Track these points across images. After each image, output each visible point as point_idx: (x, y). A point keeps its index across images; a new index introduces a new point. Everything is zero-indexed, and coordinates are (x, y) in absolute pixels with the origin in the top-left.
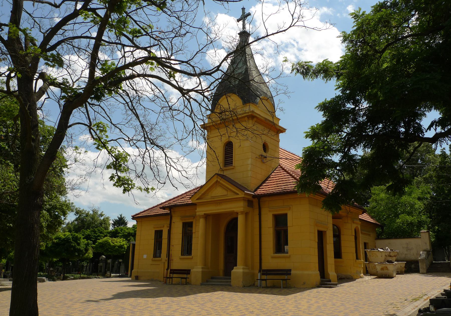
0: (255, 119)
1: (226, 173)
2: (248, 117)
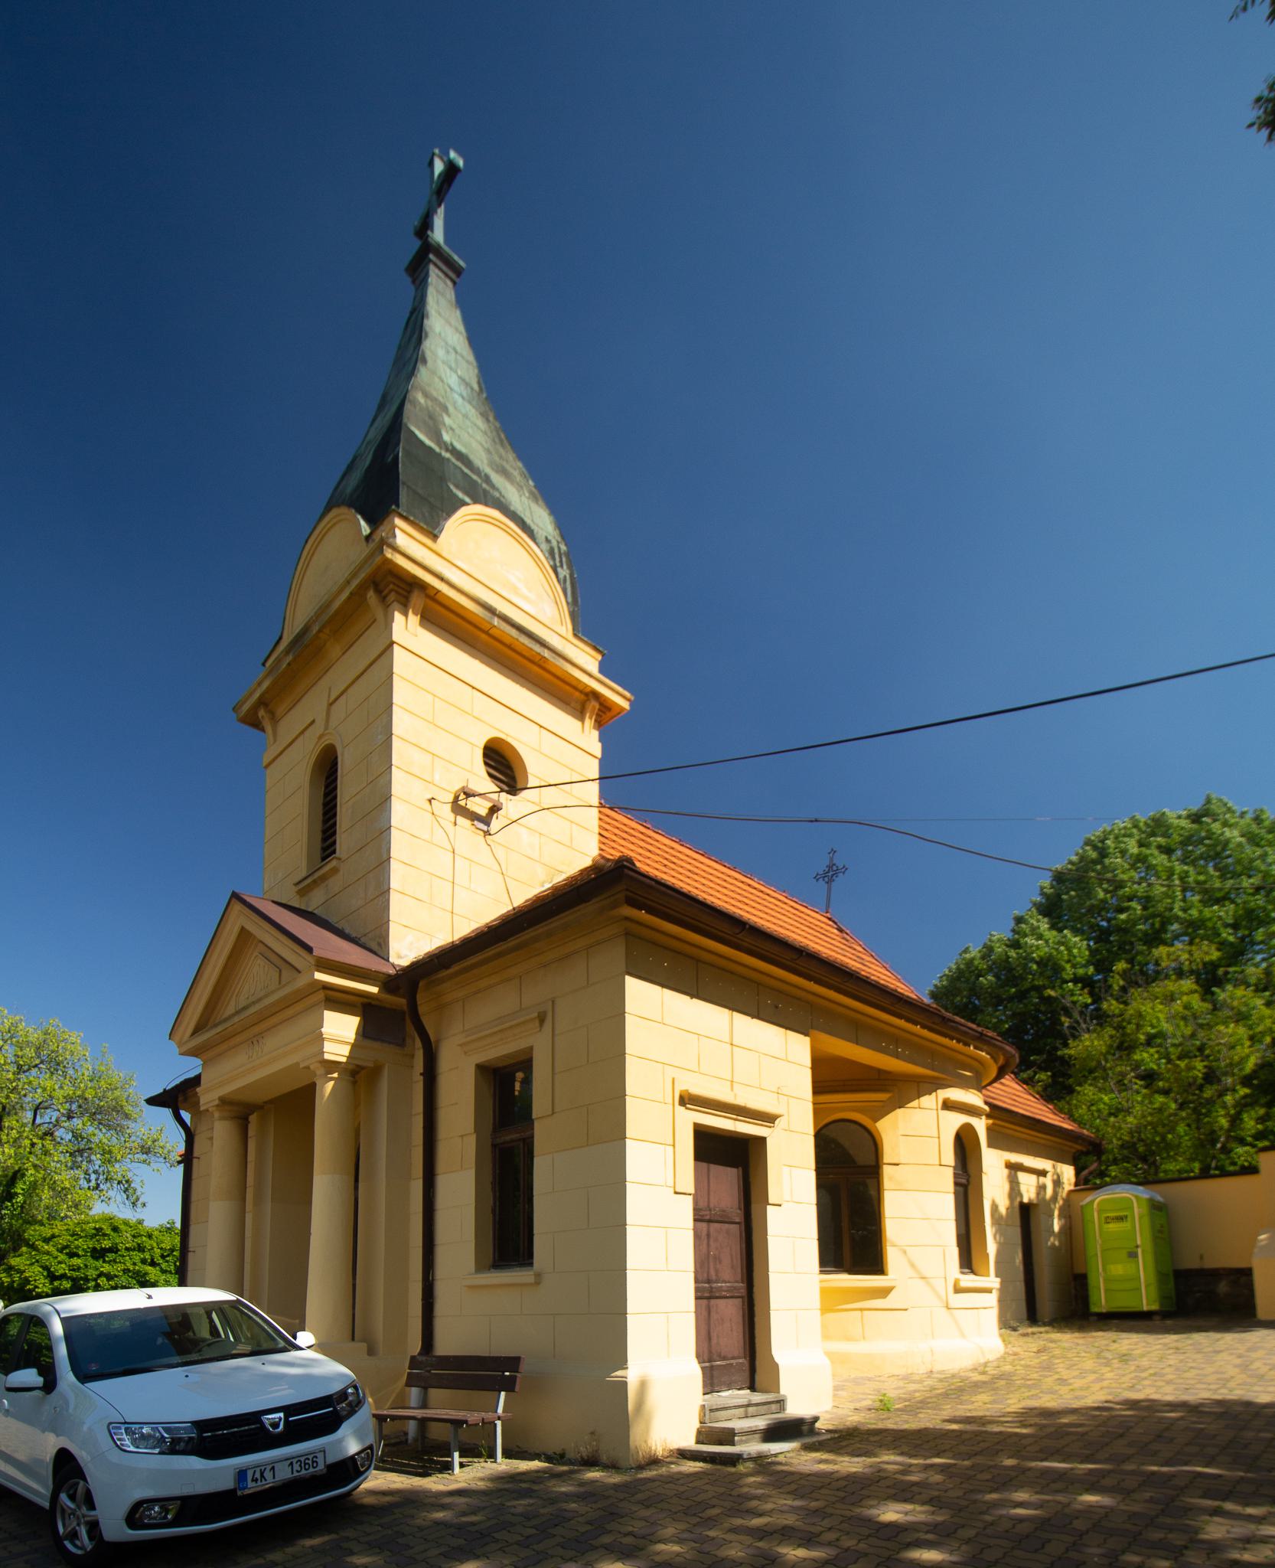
0: (417, 599)
1: (315, 902)
2: (378, 591)
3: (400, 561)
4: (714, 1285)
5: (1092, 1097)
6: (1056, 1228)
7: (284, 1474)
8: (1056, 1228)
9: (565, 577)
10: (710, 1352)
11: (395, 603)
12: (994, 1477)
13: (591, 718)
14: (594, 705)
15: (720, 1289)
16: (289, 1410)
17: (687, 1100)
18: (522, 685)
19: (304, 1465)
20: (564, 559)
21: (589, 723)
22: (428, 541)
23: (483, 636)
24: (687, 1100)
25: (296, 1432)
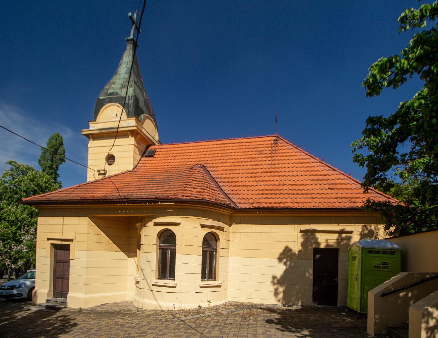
0: (90, 137)
3: (143, 131)
4: (64, 276)
5: (414, 144)
6: (376, 166)
7: (5, 294)
8: (376, 166)
9: (131, 103)
10: (62, 290)
11: (131, 140)
12: (180, 326)
13: (130, 136)
14: (129, 133)
15: (65, 277)
16: (8, 286)
17: (49, 239)
18: (103, 139)
19: (7, 293)
20: (133, 98)
21: (130, 137)
22: (95, 122)
23: (104, 134)
24: (49, 239)
25: (8, 289)
